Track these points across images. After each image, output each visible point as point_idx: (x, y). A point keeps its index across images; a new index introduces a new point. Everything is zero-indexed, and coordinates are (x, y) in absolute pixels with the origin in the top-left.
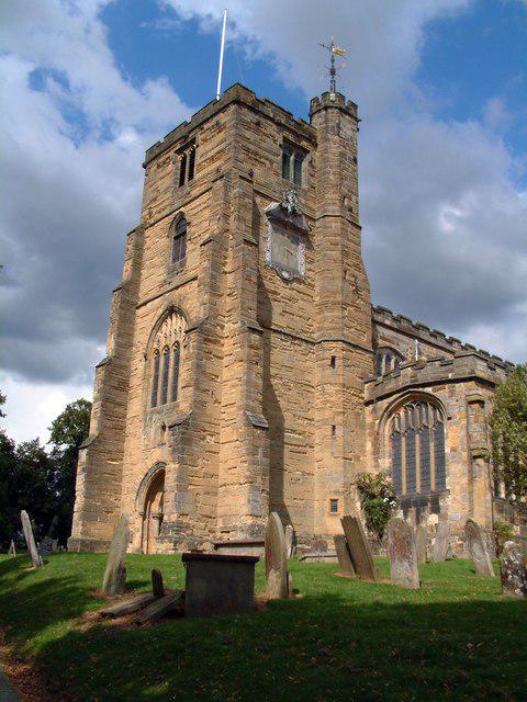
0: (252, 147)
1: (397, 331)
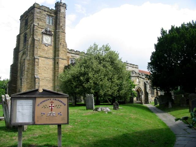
0: (39, 18)
1: (76, 54)
